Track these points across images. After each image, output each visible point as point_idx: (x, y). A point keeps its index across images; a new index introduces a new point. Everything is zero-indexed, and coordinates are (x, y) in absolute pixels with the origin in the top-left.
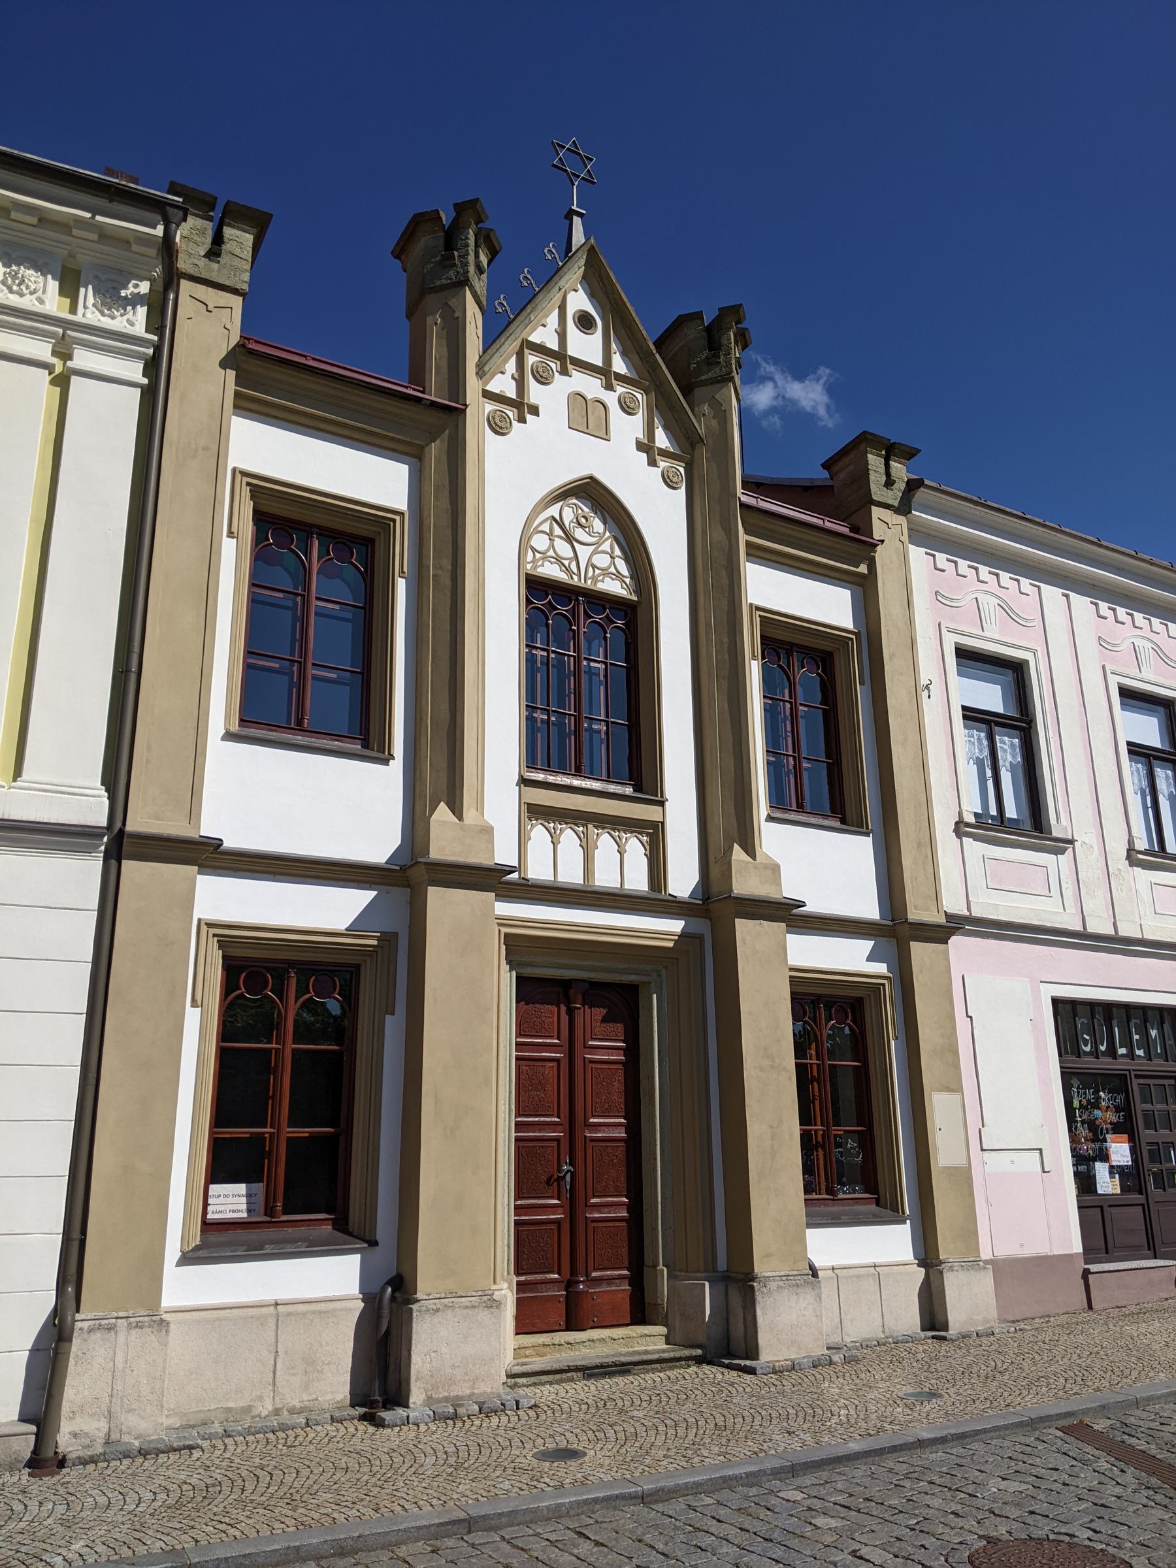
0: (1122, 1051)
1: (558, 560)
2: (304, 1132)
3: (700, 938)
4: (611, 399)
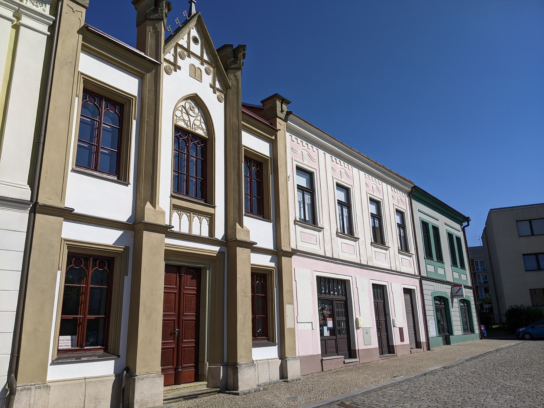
0: (332, 293)
1: (184, 120)
2: (92, 317)
3: (224, 253)
4: (203, 68)
